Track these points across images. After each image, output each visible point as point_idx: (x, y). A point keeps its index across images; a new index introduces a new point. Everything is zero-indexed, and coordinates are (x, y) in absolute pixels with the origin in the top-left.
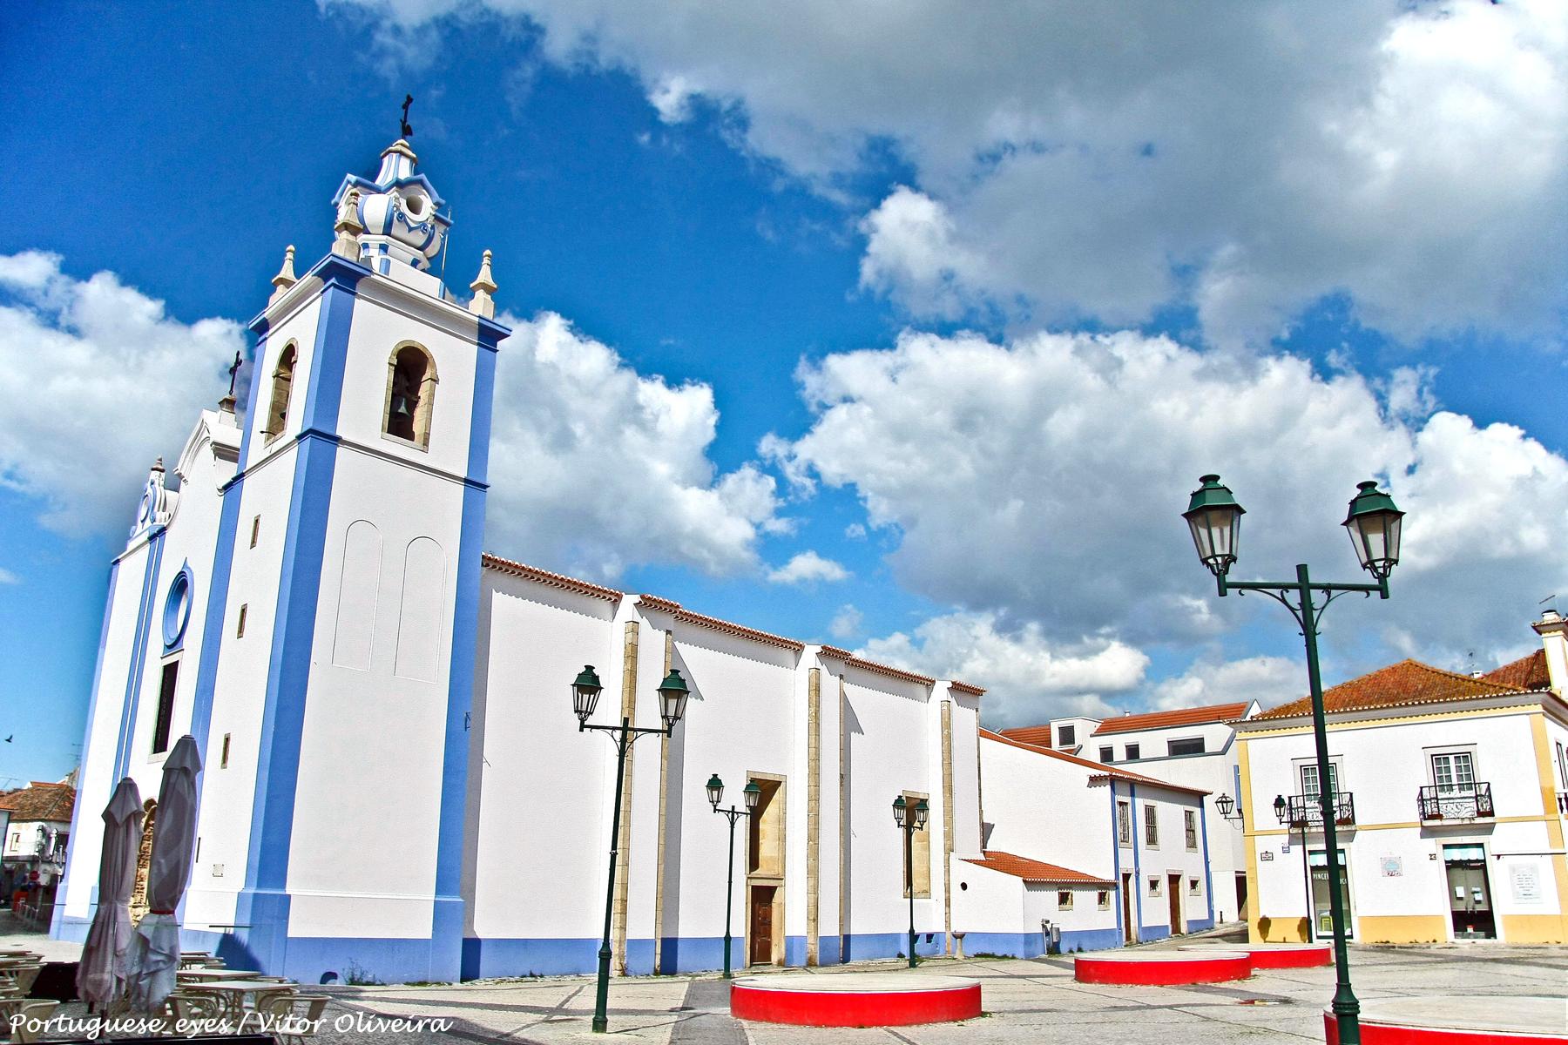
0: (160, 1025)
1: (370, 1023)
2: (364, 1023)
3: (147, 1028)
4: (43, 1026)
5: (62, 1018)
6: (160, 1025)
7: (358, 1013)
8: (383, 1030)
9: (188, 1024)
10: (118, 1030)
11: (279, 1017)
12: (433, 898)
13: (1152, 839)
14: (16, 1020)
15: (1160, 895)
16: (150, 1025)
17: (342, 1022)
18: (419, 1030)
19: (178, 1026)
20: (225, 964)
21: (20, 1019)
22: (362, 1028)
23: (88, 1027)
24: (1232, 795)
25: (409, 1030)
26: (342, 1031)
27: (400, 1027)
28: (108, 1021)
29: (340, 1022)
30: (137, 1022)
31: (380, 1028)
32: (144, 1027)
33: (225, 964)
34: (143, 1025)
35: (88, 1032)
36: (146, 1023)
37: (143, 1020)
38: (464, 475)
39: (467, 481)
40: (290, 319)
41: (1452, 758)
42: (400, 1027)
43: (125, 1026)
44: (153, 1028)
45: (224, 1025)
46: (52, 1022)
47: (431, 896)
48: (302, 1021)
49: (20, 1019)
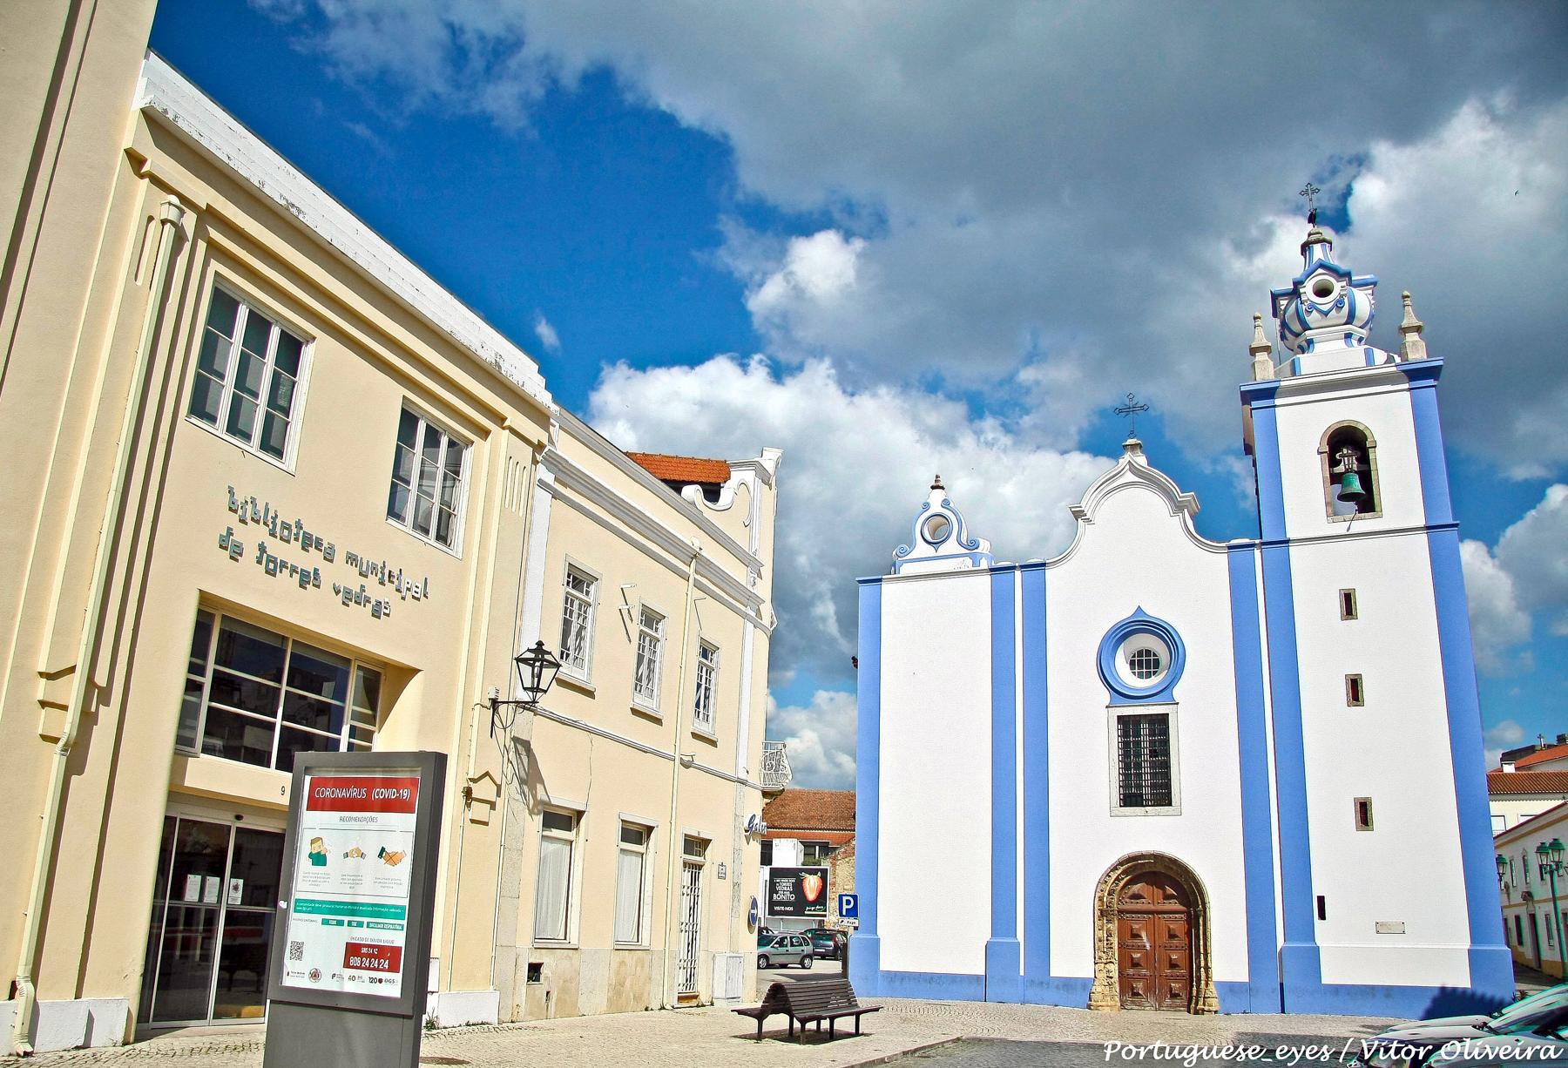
3: (1247, 1055)
4: (1138, 1053)
8: (1491, 1057)
9: (1289, 1051)
12: (1468, 947)
13: (1322, 916)
15: (1546, 884)
18: (1528, 1058)
20: (792, 909)
24: (553, 646)
25: (1553, 1057)
26: (1447, 1058)
30: (1320, 1048)
31: (1487, 1055)
32: (1243, 1055)
33: (792, 909)
34: (1242, 1052)
35: (1184, 1059)
36: (1245, 1050)
38: (1422, 523)
39: (1428, 528)
46: (1148, 1049)
47: (1467, 944)
48: (1406, 1048)
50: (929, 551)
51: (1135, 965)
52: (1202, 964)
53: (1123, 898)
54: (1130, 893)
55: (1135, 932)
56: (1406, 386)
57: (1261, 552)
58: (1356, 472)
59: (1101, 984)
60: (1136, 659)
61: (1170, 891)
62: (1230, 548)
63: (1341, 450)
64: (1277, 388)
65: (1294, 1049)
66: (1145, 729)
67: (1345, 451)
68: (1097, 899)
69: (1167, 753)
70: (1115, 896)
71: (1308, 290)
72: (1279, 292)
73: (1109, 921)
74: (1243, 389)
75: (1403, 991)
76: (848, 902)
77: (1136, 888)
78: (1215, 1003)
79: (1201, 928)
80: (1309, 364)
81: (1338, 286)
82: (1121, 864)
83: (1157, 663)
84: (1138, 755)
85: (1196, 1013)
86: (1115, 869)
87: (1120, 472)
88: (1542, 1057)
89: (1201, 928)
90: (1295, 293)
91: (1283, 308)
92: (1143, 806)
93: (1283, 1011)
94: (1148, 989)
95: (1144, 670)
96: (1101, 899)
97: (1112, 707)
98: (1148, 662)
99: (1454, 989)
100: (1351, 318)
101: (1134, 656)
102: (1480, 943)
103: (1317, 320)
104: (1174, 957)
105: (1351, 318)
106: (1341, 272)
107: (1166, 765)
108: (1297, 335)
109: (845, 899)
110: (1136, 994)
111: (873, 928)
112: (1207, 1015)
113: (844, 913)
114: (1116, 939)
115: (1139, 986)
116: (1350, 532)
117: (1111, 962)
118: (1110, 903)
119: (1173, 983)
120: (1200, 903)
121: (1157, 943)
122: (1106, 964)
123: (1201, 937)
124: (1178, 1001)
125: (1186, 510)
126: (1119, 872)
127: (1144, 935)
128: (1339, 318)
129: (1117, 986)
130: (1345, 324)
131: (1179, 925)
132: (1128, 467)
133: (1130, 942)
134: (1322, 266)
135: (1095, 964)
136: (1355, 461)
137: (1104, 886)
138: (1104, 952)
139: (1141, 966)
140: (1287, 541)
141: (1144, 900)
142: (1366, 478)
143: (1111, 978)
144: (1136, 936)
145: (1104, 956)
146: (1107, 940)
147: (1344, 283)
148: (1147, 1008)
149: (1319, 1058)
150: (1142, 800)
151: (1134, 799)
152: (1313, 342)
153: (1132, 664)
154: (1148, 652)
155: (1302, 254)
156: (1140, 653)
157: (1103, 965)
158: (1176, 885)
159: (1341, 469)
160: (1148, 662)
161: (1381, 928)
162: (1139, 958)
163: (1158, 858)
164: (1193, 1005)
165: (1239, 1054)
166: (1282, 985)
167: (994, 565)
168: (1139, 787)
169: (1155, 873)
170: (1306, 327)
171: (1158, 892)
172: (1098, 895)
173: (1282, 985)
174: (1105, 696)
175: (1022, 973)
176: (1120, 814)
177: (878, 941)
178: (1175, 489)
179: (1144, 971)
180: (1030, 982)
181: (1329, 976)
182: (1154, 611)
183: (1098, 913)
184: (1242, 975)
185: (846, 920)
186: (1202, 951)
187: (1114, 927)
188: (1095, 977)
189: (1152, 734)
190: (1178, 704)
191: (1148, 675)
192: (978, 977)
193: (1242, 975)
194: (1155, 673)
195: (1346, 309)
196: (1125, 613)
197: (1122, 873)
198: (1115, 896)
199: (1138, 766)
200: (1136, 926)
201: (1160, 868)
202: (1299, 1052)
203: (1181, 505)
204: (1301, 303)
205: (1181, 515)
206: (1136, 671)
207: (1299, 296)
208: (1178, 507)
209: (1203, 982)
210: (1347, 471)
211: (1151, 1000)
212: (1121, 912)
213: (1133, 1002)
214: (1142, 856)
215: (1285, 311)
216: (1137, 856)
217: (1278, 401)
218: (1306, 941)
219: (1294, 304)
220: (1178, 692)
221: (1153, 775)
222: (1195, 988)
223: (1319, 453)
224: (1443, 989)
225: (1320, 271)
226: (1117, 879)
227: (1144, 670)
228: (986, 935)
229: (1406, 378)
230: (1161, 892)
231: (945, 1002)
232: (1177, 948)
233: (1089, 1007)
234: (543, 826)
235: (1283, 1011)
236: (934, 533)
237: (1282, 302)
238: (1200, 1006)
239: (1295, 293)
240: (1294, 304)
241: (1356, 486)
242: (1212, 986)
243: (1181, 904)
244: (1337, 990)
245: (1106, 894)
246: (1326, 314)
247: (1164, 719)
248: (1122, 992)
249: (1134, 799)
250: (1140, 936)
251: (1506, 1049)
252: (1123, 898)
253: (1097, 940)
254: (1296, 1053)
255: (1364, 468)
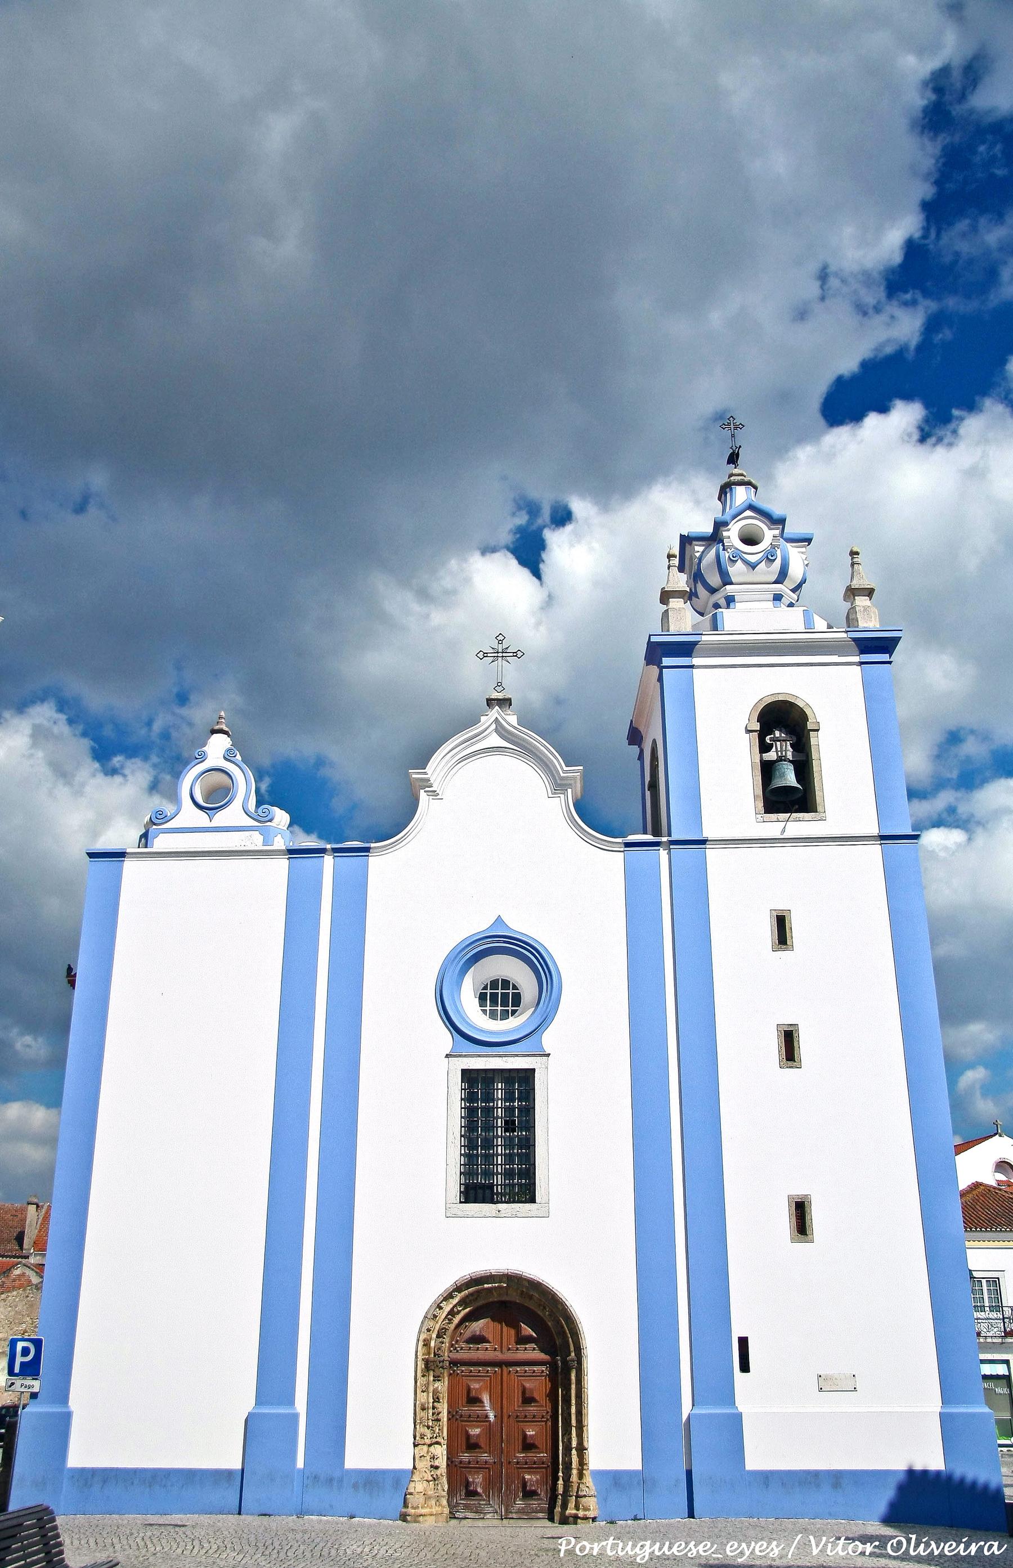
0: (710, 1549)
1: (922, 1546)
2: (917, 1546)
3: (698, 1552)
5: (611, 1541)
6: (710, 1549)
7: (910, 1536)
8: (936, 1553)
10: (841, 1553)
11: (831, 1540)
12: (939, 1410)
13: (745, 1367)
14: (564, 1543)
16: (701, 1548)
17: (895, 1545)
18: (973, 1554)
19: (728, 1549)
21: (569, 1543)
22: (831, 1552)
23: (637, 1550)
27: (953, 1550)
28: (658, 1544)
29: (892, 1544)
32: (694, 1551)
34: (693, 1548)
35: (636, 1555)
37: (693, 1543)
40: (342, 856)
41: (984, 1281)
42: (953, 1550)
43: (675, 1550)
44: (760, 1551)
45: (775, 1548)
47: (934, 1405)
49: (569, 1543)
50: (201, 819)
51: (472, 1446)
52: (574, 1444)
53: (457, 1341)
54: (468, 1334)
55: (473, 1394)
56: (856, 659)
57: (669, 854)
58: (790, 761)
59: (422, 1479)
60: (489, 991)
61: (527, 1330)
62: (628, 845)
63: (771, 732)
64: (695, 643)
65: (744, 1545)
66: (499, 1090)
67: (777, 734)
68: (421, 1343)
69: (529, 1126)
70: (447, 1340)
71: (732, 534)
72: (694, 535)
73: (437, 1378)
74: (653, 639)
75: (837, 1479)
76: (25, 1352)
77: (477, 1326)
78: (592, 1505)
79: (573, 1386)
80: (732, 620)
81: (769, 535)
82: (458, 1289)
83: (517, 999)
84: (489, 1127)
85: (564, 1521)
86: (449, 1296)
87: (486, 730)
88: (986, 1553)
89: (573, 1386)
90: (715, 538)
91: (698, 555)
92: (492, 1202)
93: (691, 1515)
94: (491, 1484)
95: (499, 1008)
96: (426, 1343)
97: (455, 1056)
98: (505, 996)
99: (925, 1472)
100: (782, 576)
101: (485, 988)
102: (958, 1402)
103: (740, 574)
104: (530, 1433)
105: (782, 576)
106: (775, 517)
107: (528, 1144)
108: (713, 591)
109: (20, 1345)
110: (471, 1494)
111: (63, 1397)
112: (581, 1525)
113: (17, 1370)
114: (446, 1406)
115: (477, 1480)
116: (786, 835)
117: (438, 1443)
118: (439, 1349)
119: (529, 1473)
120: (572, 1348)
121: (505, 1411)
122: (430, 1445)
123: (573, 1402)
124: (534, 1503)
125: (570, 790)
126: (455, 1301)
127: (486, 1398)
128: (769, 573)
129: (445, 1480)
130: (775, 582)
131: (538, 1384)
132: (494, 726)
133: (465, 1410)
134: (751, 507)
135: (415, 1445)
136: (789, 748)
137: (431, 1323)
138: (428, 1427)
139: (480, 1447)
140: (703, 842)
141: (487, 1345)
142: (804, 768)
143: (437, 1468)
144: (474, 1400)
145: (428, 1433)
146: (434, 1408)
147: (777, 532)
148: (488, 1516)
149: (686, 1554)
150: (493, 1193)
151: (480, 1192)
152: (734, 601)
153: (482, 998)
154: (506, 983)
155: (720, 499)
156: (494, 984)
157: (425, 1448)
158: (536, 1322)
159: (771, 756)
160: (505, 996)
161: (824, 1384)
162: (478, 1436)
163: (514, 1281)
164: (558, 1509)
165: (690, 1550)
166: (689, 1473)
167: (292, 846)
168: (488, 1174)
169: (503, 1303)
170: (727, 581)
171: (509, 1333)
172: (423, 1337)
173: (689, 1473)
174: (445, 1040)
175: (300, 1464)
176: (460, 1213)
177: (68, 1416)
178: (558, 762)
179: (485, 1457)
180: (312, 1478)
181: (755, 1460)
182: (520, 925)
183: (421, 1365)
184: (632, 1460)
185: (18, 1382)
186: (574, 1422)
187: (442, 1386)
188: (415, 1468)
189: (509, 1097)
190: (548, 1055)
191: (505, 1016)
192: (229, 1473)
193: (632, 1460)
194: (514, 1012)
195: (777, 564)
196: (479, 924)
197: (459, 1303)
198: (447, 1340)
199: (488, 1144)
200: (474, 1386)
201: (514, 1297)
202: (938, 1548)
203: (564, 782)
204: (724, 549)
205: (562, 796)
206: (488, 1008)
207: (722, 541)
208: (559, 786)
209: (575, 1472)
210: (780, 759)
211: (495, 1502)
212: (454, 1363)
213: (467, 1507)
214: (490, 1278)
215: (700, 559)
216: (481, 1278)
217: (696, 661)
218: (715, 1403)
219: (713, 551)
220: (549, 1039)
221: (509, 1158)
222: (561, 1482)
223: (748, 731)
224: (911, 1473)
225: (748, 513)
226: (452, 1313)
227: (499, 1008)
228: (247, 1402)
229: (856, 650)
230: (513, 1332)
231: (176, 1518)
232: (534, 1419)
233: (403, 1517)
234: (941, 1023)
235: (691, 1515)
236: (209, 796)
237: (697, 548)
238: (571, 1511)
239: (715, 538)
240: (713, 551)
241: (790, 778)
242: (588, 1479)
243: (542, 1350)
244: (766, 1477)
245: (434, 1336)
246: (753, 566)
247: (527, 1077)
248: (451, 1493)
249: (480, 1192)
250: (481, 1401)
251: (951, 1545)
252: (457, 1341)
253: (420, 1408)
254: (746, 1549)
255: (801, 757)
